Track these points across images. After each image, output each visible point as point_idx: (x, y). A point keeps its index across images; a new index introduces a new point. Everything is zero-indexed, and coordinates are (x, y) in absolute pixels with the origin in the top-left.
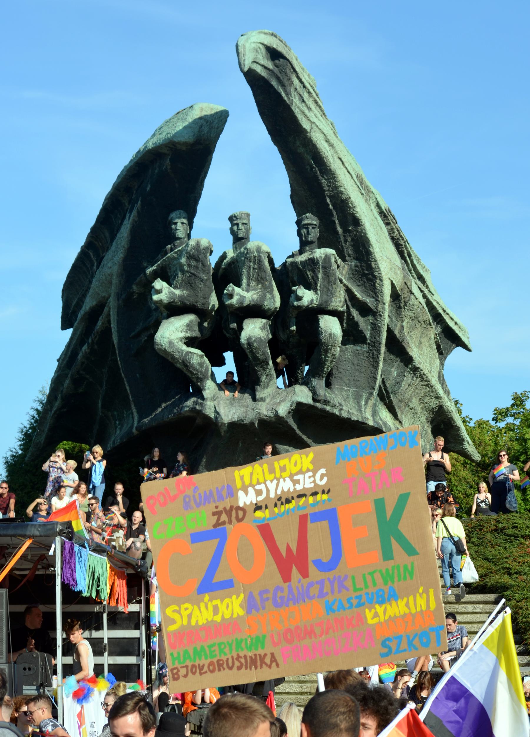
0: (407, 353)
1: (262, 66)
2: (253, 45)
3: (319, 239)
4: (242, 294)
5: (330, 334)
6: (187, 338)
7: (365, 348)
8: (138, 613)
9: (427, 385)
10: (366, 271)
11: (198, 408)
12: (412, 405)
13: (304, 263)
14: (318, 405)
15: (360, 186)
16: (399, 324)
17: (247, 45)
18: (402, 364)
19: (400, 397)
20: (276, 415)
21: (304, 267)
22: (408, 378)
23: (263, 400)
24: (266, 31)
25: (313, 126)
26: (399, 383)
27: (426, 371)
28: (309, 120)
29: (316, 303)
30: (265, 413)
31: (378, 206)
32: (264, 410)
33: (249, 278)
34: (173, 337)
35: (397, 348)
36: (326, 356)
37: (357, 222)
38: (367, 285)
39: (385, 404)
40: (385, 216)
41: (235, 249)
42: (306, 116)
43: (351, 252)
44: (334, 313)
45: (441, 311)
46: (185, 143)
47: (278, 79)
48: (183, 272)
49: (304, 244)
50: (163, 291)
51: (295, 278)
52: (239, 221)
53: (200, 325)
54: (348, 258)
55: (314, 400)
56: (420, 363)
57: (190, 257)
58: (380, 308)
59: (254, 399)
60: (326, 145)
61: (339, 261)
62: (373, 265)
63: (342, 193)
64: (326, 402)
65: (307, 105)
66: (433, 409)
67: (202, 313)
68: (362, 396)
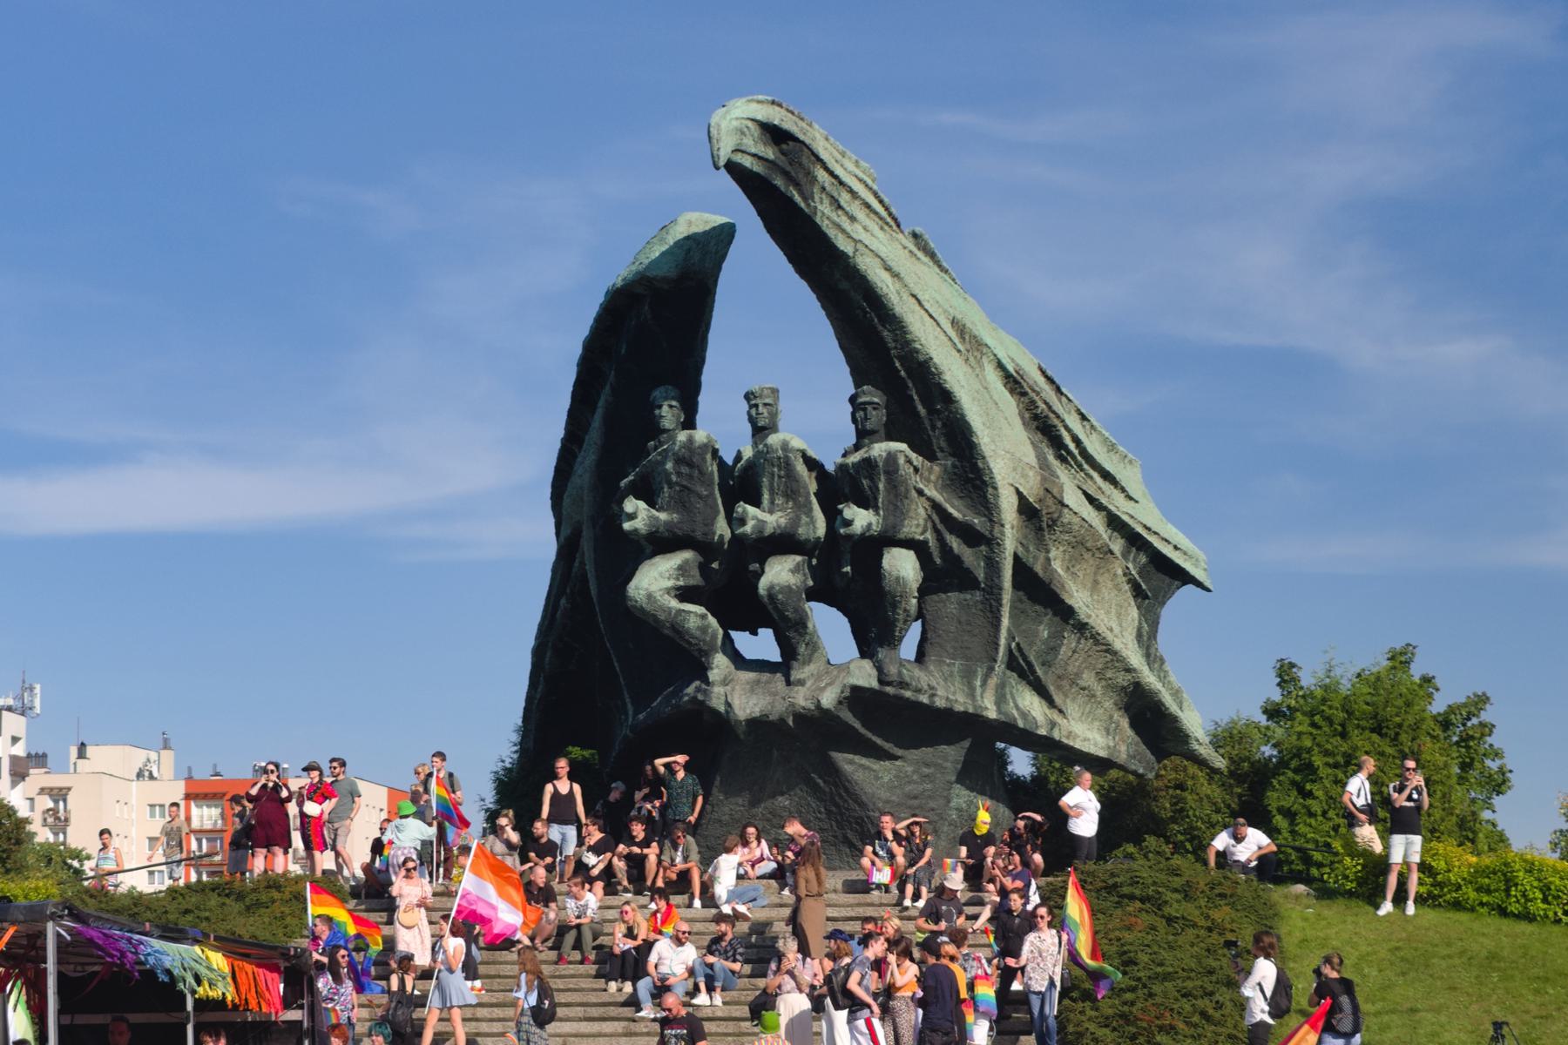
0: (1063, 601)
1: (754, 155)
2: (735, 123)
3: (886, 425)
4: (761, 518)
5: (898, 578)
6: (678, 588)
7: (978, 596)
8: (301, 1022)
9: (1107, 651)
10: (970, 474)
11: (700, 697)
12: (1082, 683)
13: (856, 465)
14: (889, 689)
15: (956, 340)
16: (1042, 556)
17: (724, 125)
18: (1057, 619)
19: (1059, 672)
20: (818, 706)
21: (857, 472)
22: (1070, 640)
23: (801, 683)
24: (760, 97)
25: (859, 246)
26: (1054, 650)
27: (1102, 629)
28: (850, 237)
29: (876, 528)
30: (802, 703)
31: (1000, 366)
32: (801, 698)
33: (772, 492)
34: (653, 588)
35: (1039, 591)
36: (894, 612)
37: (947, 397)
38: (974, 495)
39: (1030, 683)
40: (1016, 382)
41: (755, 445)
42: (843, 231)
43: (943, 444)
44: (908, 544)
45: (1140, 529)
46: (664, 279)
47: (786, 175)
48: (671, 485)
49: (864, 435)
50: (639, 515)
51: (847, 490)
52: (758, 401)
53: (704, 568)
54: (939, 455)
55: (881, 681)
56: (1089, 616)
57: (680, 461)
58: (996, 532)
59: (788, 683)
60: (885, 276)
61: (917, 459)
62: (980, 465)
63: (917, 351)
64: (903, 684)
65: (847, 213)
66: (1124, 688)
67: (706, 549)
68: (975, 672)
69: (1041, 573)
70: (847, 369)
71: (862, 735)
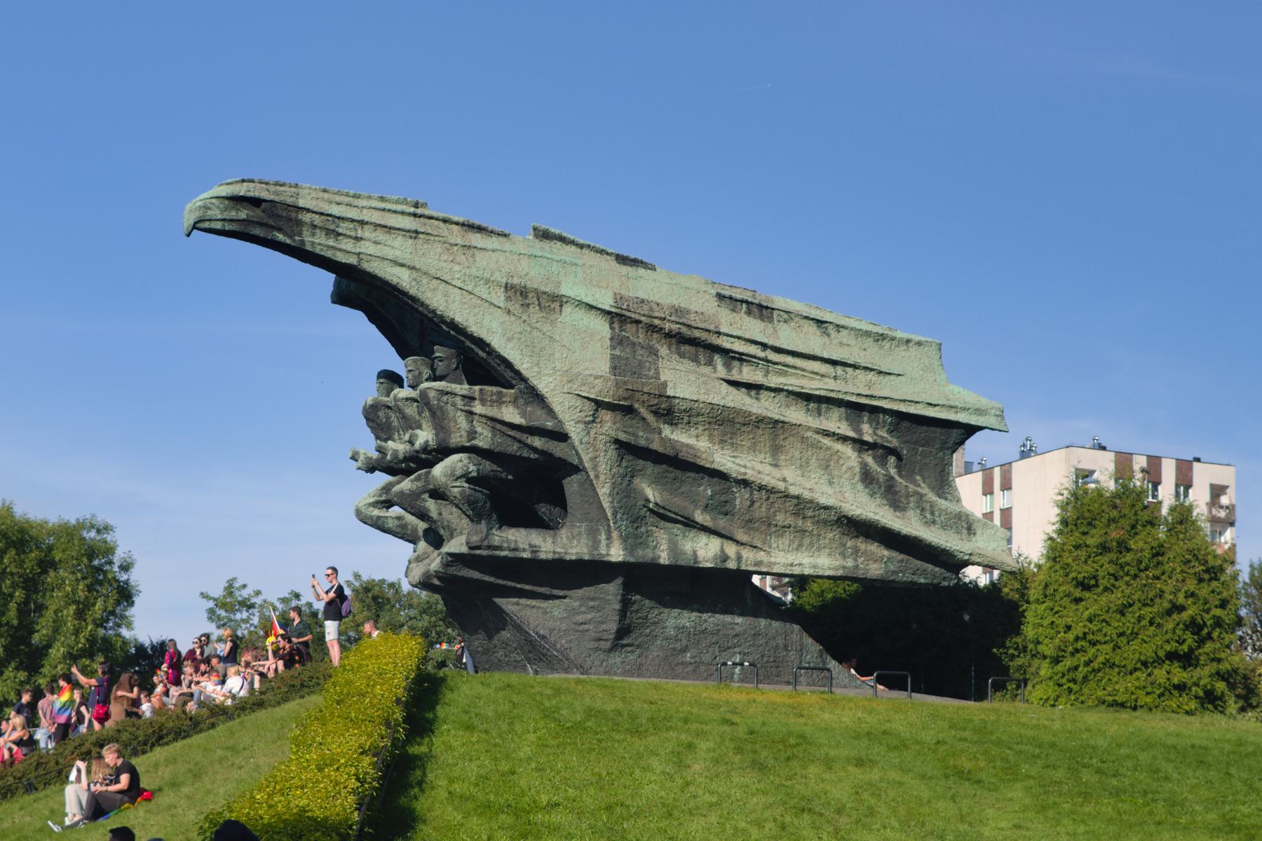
60: (397, 271)
68: (598, 530)
69: (661, 450)
70: (393, 350)
71: (499, 585)
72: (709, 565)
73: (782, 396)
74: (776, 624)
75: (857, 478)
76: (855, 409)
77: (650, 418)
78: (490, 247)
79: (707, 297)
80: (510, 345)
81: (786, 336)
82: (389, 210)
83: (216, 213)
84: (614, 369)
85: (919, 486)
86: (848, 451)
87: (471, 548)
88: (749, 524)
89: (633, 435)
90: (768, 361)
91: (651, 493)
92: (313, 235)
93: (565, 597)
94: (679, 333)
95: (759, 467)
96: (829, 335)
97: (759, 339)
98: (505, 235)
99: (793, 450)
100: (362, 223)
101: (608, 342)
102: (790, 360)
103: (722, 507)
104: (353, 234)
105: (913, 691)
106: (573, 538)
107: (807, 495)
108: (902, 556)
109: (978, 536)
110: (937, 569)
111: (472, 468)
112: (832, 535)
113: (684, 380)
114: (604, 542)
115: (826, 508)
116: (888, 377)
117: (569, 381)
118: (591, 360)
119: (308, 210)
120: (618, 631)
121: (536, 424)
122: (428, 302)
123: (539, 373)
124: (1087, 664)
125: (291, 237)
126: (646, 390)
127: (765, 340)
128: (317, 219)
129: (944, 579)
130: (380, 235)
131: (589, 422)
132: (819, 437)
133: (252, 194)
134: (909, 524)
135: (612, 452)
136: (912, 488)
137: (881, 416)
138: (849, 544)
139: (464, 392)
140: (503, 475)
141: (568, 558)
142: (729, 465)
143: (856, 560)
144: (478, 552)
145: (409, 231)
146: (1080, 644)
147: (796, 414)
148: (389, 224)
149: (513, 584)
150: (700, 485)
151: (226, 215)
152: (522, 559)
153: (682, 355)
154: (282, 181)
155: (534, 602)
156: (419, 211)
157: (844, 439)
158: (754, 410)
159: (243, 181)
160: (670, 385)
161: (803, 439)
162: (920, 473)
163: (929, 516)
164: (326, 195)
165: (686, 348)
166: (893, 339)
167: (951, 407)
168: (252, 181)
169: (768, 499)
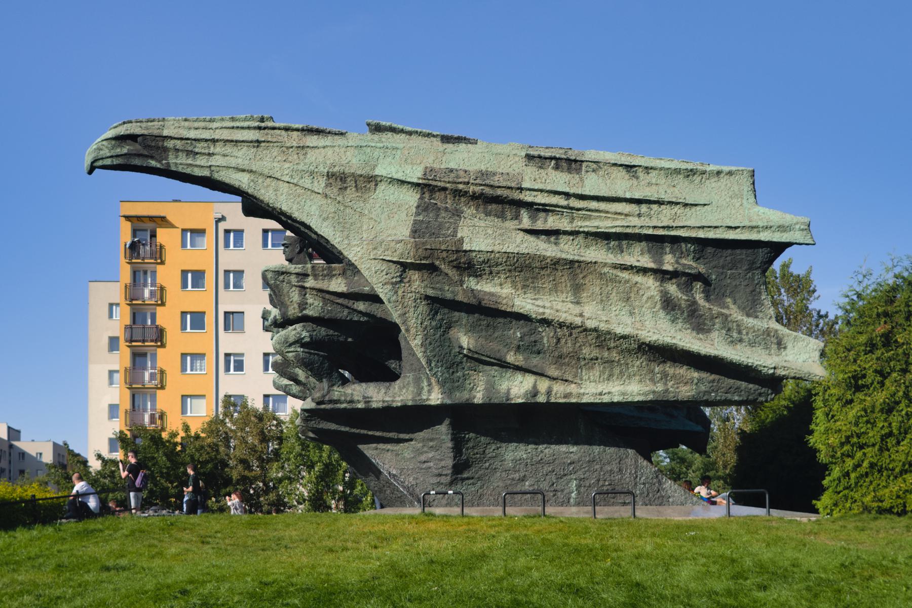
68: (420, 378)
69: (465, 300)
72: (520, 401)
73: (580, 238)
74: (611, 450)
75: (658, 306)
76: (657, 241)
77: (451, 272)
78: (320, 145)
79: (517, 159)
80: (325, 224)
81: (592, 184)
82: (238, 127)
83: (106, 152)
84: (415, 232)
85: (728, 308)
86: (650, 284)
87: (318, 403)
88: (559, 360)
89: (440, 289)
90: (572, 208)
91: (465, 340)
92: (177, 157)
93: (411, 440)
94: (482, 194)
95: (559, 306)
96: (637, 178)
97: (560, 189)
98: (342, 134)
99: (593, 287)
100: (214, 141)
101: (414, 210)
102: (594, 205)
103: (532, 347)
104: (207, 151)
105: (771, 507)
106: (404, 387)
107: (603, 327)
108: (713, 377)
109: (788, 351)
110: (751, 386)
111: (304, 334)
112: (638, 362)
113: (479, 234)
114: (426, 389)
115: (624, 337)
116: (694, 209)
117: (375, 249)
118: (394, 228)
119: (172, 138)
120: (454, 466)
121: (356, 290)
122: (261, 198)
123: (349, 244)
124: (857, 466)
125: (160, 162)
126: (443, 247)
127: (567, 190)
128: (179, 144)
129: (760, 394)
130: (229, 149)
131: (396, 283)
132: (615, 272)
133: (128, 132)
134: (714, 345)
135: (423, 308)
136: (716, 309)
137: (683, 245)
138: (657, 369)
139: (297, 271)
140: (342, 339)
141: (394, 405)
142: (529, 307)
143: (666, 384)
144: (323, 406)
145: (251, 142)
146: (847, 448)
147: (596, 254)
148: (235, 139)
149: (365, 432)
150: (510, 329)
151: (113, 153)
152: (358, 409)
153: (488, 214)
154: (152, 118)
155: (389, 446)
156: (263, 125)
157: (644, 271)
158: (548, 254)
159: (124, 123)
160: (466, 240)
161: (601, 276)
162: (732, 295)
163: (735, 335)
164: (187, 124)
165: (493, 207)
166: (704, 173)
167: (753, 227)
168: (130, 122)
169: (571, 334)
